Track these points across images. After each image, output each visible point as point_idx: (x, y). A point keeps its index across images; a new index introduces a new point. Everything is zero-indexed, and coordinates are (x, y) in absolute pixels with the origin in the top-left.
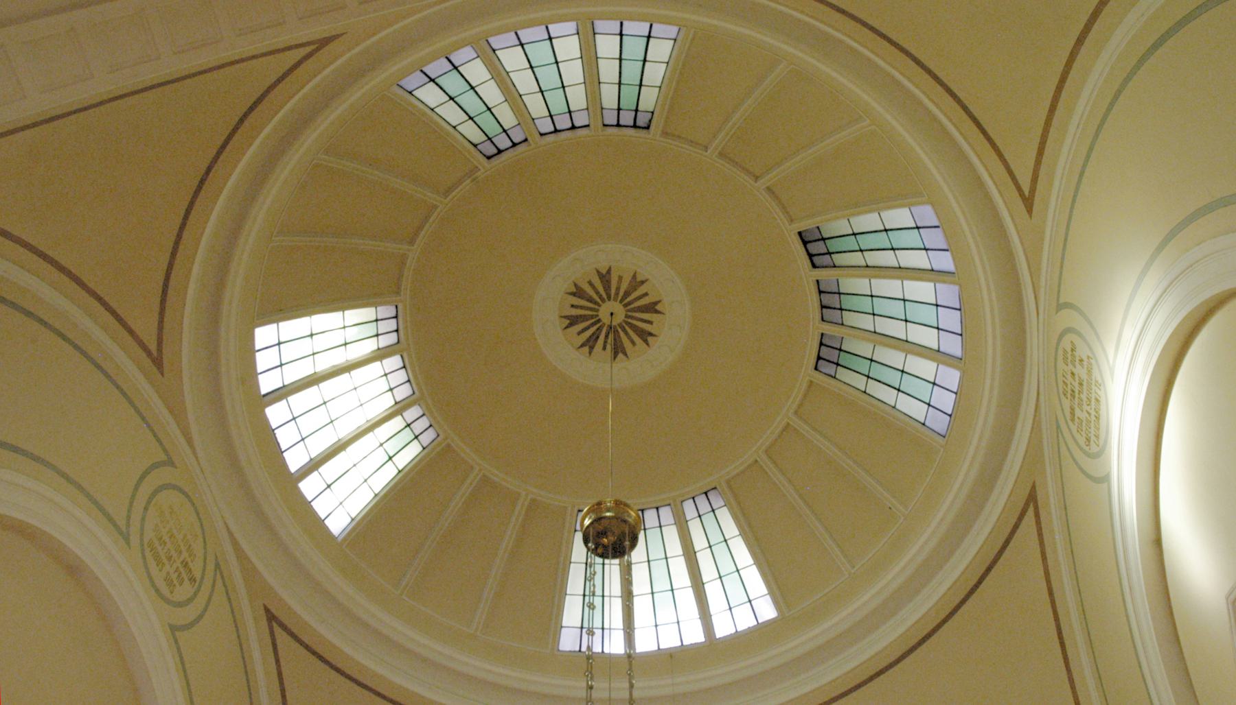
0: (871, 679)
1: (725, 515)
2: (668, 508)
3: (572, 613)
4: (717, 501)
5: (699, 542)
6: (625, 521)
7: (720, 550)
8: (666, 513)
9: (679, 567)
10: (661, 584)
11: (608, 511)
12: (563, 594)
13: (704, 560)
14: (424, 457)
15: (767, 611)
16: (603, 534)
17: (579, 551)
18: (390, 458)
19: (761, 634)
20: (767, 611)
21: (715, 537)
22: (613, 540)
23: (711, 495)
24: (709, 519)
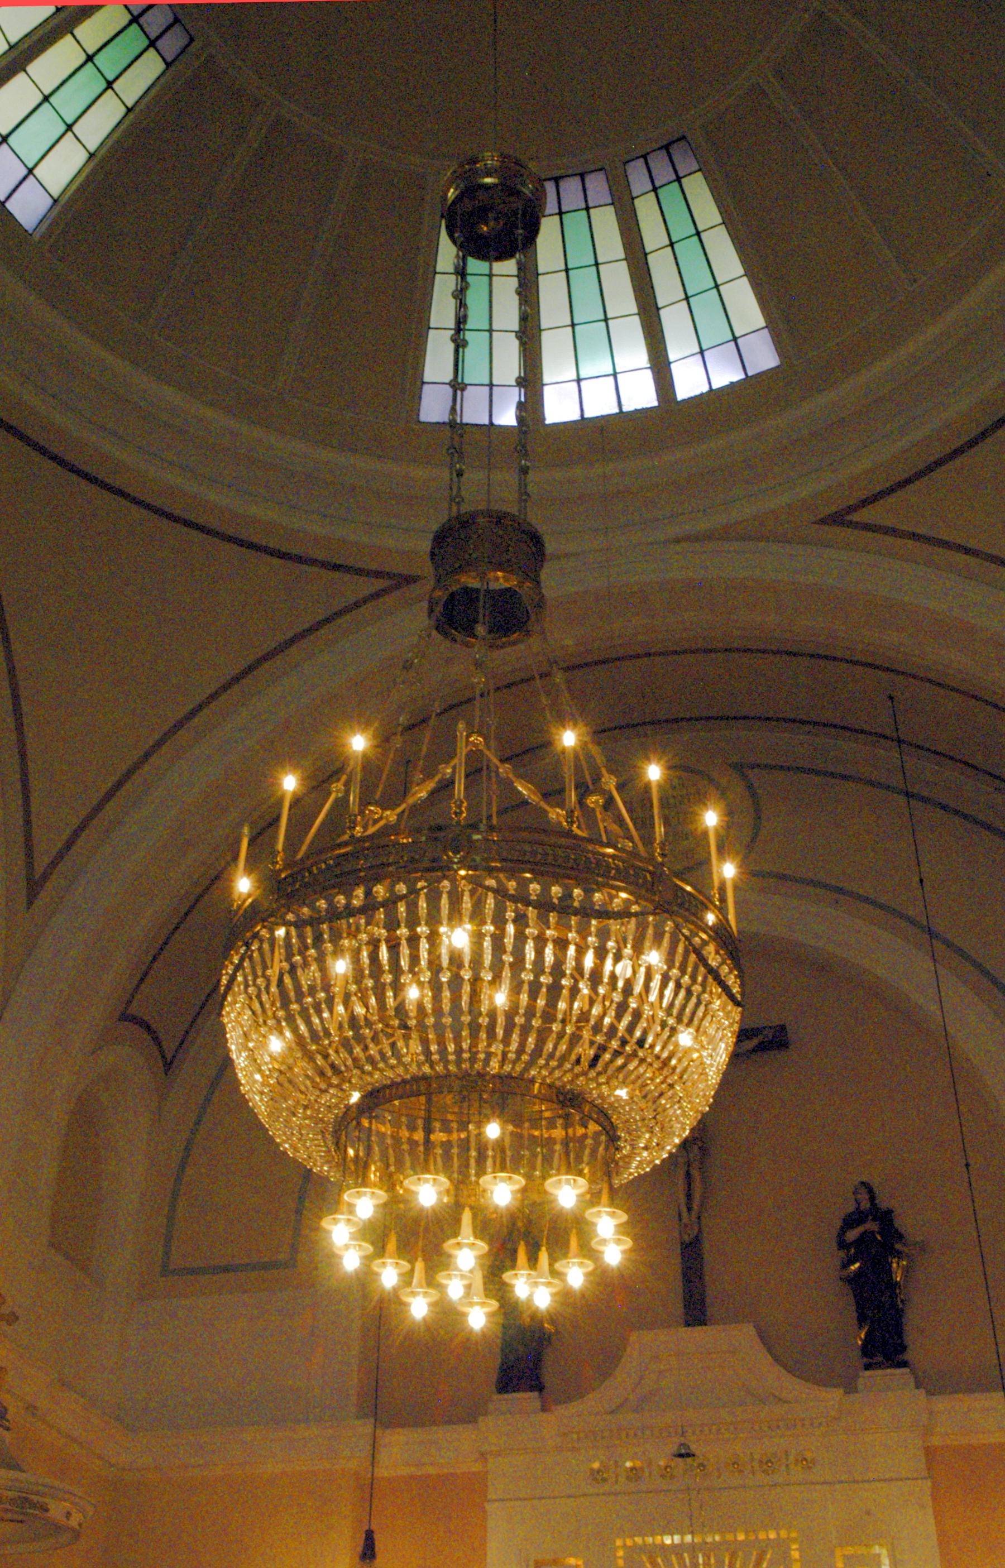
0: (677, 264)
1: (697, 186)
2: (601, 176)
3: (437, 362)
4: (685, 163)
5: (653, 236)
6: (518, 193)
7: (688, 250)
8: (597, 185)
9: (618, 279)
10: (588, 309)
11: (488, 175)
12: (422, 327)
13: (660, 266)
14: (93, 172)
15: (764, 357)
16: (482, 213)
17: (447, 253)
18: (69, 127)
19: (750, 391)
20: (764, 357)
21: (681, 228)
22: (500, 227)
23: (676, 151)
24: (670, 194)
